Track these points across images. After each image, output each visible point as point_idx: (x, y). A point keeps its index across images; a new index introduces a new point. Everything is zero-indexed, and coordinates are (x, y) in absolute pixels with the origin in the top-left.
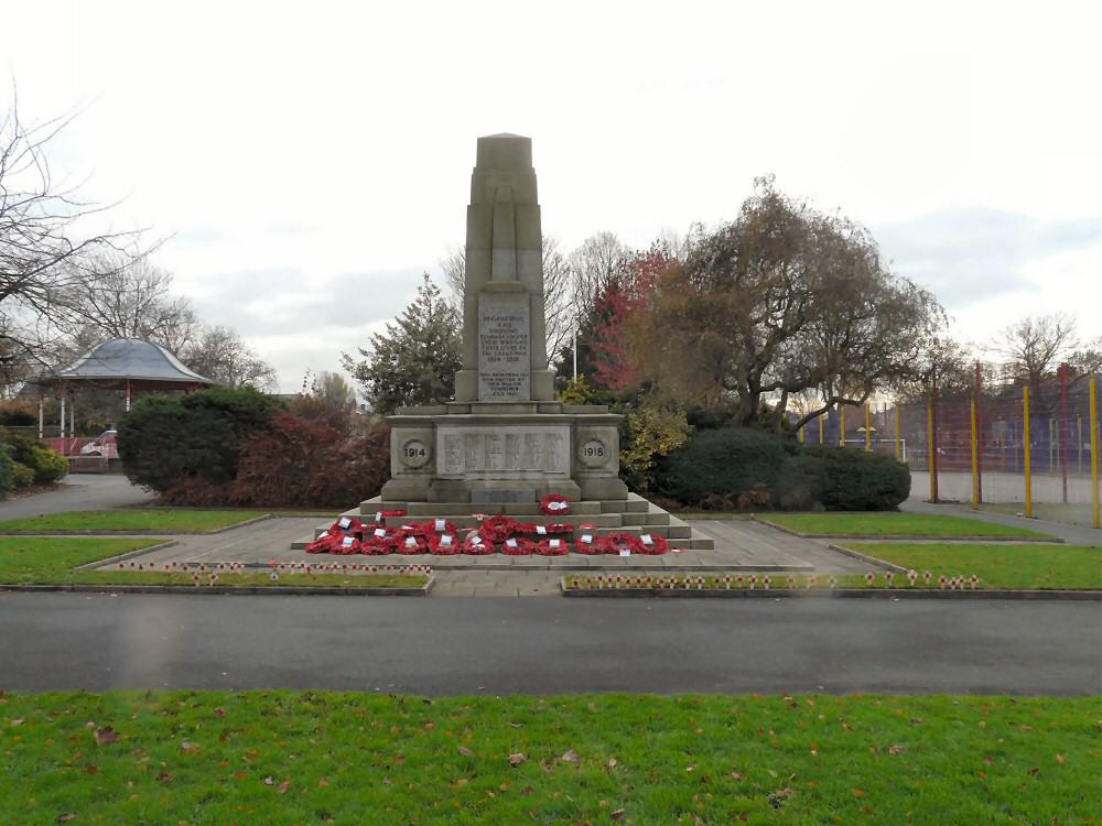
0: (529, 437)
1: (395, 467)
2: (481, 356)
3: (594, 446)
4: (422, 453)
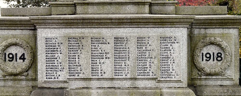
0: (140, 40)
3: (213, 50)
4: (23, 58)
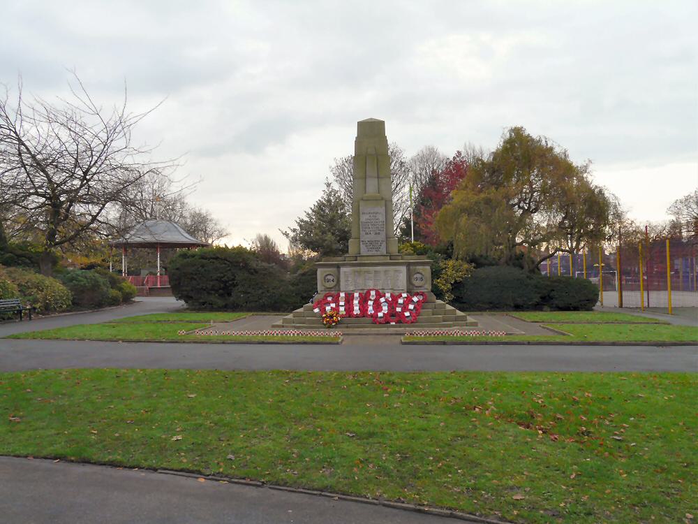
0: (386, 271)
1: (319, 288)
2: (361, 232)
